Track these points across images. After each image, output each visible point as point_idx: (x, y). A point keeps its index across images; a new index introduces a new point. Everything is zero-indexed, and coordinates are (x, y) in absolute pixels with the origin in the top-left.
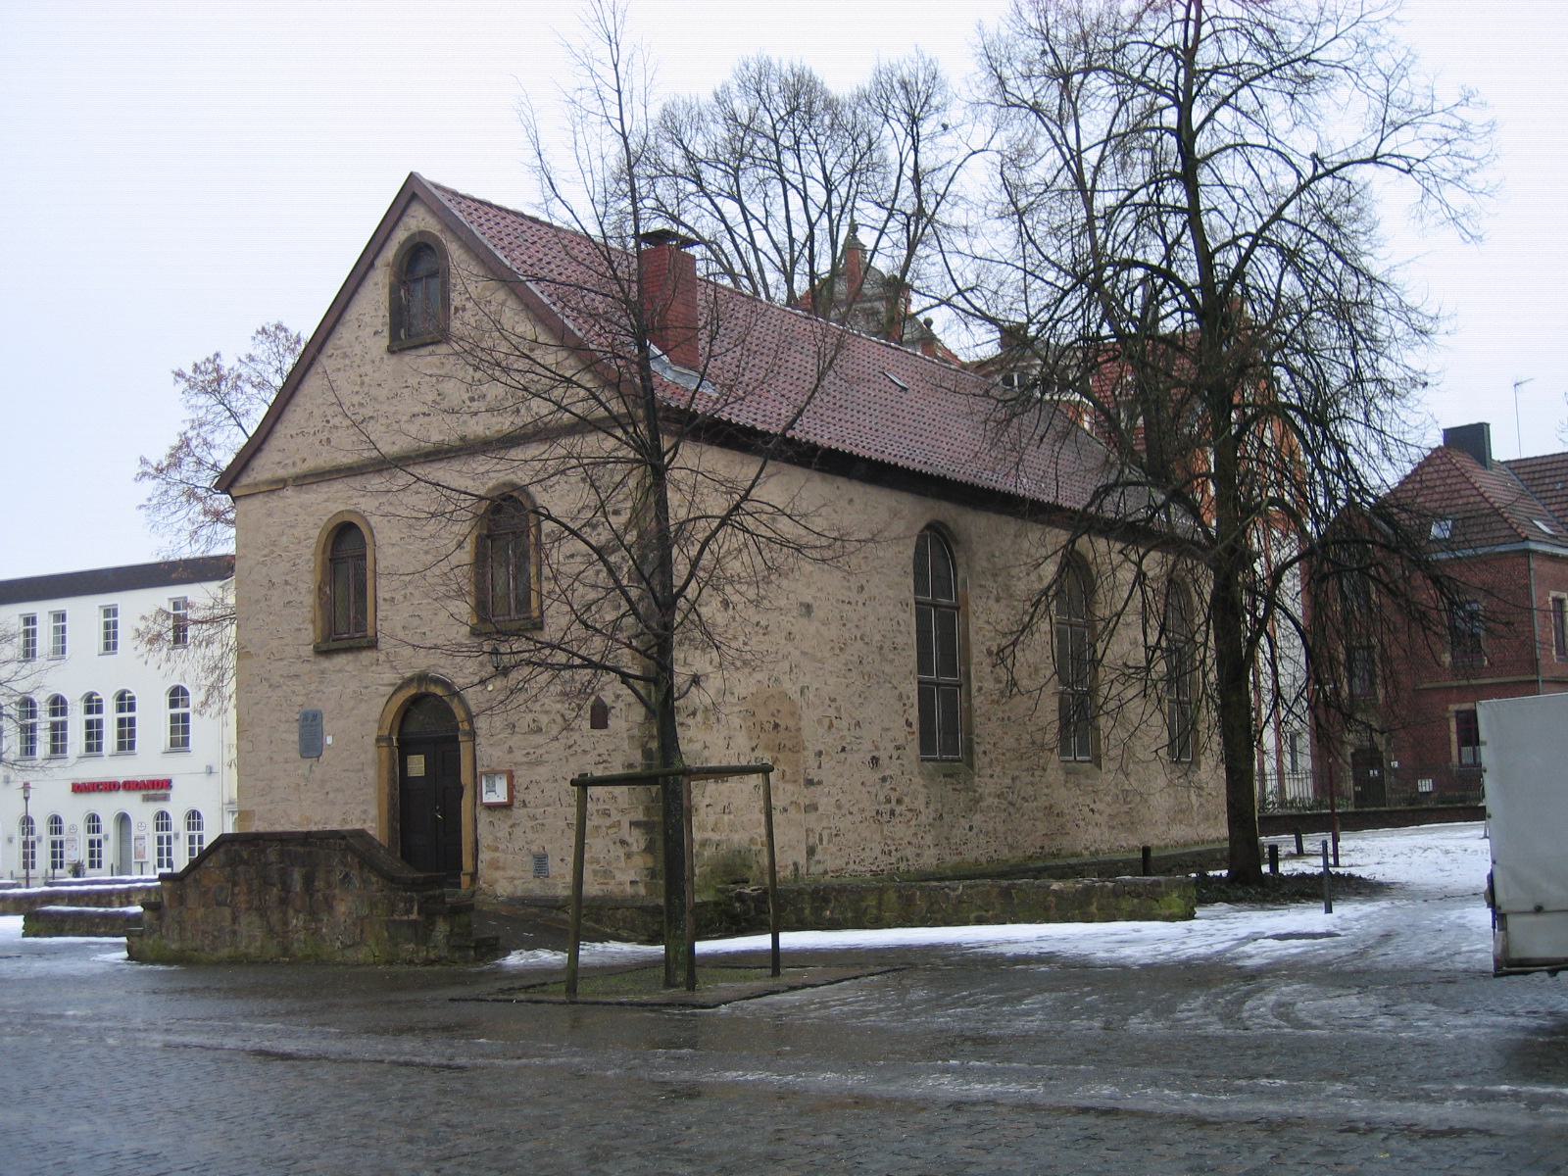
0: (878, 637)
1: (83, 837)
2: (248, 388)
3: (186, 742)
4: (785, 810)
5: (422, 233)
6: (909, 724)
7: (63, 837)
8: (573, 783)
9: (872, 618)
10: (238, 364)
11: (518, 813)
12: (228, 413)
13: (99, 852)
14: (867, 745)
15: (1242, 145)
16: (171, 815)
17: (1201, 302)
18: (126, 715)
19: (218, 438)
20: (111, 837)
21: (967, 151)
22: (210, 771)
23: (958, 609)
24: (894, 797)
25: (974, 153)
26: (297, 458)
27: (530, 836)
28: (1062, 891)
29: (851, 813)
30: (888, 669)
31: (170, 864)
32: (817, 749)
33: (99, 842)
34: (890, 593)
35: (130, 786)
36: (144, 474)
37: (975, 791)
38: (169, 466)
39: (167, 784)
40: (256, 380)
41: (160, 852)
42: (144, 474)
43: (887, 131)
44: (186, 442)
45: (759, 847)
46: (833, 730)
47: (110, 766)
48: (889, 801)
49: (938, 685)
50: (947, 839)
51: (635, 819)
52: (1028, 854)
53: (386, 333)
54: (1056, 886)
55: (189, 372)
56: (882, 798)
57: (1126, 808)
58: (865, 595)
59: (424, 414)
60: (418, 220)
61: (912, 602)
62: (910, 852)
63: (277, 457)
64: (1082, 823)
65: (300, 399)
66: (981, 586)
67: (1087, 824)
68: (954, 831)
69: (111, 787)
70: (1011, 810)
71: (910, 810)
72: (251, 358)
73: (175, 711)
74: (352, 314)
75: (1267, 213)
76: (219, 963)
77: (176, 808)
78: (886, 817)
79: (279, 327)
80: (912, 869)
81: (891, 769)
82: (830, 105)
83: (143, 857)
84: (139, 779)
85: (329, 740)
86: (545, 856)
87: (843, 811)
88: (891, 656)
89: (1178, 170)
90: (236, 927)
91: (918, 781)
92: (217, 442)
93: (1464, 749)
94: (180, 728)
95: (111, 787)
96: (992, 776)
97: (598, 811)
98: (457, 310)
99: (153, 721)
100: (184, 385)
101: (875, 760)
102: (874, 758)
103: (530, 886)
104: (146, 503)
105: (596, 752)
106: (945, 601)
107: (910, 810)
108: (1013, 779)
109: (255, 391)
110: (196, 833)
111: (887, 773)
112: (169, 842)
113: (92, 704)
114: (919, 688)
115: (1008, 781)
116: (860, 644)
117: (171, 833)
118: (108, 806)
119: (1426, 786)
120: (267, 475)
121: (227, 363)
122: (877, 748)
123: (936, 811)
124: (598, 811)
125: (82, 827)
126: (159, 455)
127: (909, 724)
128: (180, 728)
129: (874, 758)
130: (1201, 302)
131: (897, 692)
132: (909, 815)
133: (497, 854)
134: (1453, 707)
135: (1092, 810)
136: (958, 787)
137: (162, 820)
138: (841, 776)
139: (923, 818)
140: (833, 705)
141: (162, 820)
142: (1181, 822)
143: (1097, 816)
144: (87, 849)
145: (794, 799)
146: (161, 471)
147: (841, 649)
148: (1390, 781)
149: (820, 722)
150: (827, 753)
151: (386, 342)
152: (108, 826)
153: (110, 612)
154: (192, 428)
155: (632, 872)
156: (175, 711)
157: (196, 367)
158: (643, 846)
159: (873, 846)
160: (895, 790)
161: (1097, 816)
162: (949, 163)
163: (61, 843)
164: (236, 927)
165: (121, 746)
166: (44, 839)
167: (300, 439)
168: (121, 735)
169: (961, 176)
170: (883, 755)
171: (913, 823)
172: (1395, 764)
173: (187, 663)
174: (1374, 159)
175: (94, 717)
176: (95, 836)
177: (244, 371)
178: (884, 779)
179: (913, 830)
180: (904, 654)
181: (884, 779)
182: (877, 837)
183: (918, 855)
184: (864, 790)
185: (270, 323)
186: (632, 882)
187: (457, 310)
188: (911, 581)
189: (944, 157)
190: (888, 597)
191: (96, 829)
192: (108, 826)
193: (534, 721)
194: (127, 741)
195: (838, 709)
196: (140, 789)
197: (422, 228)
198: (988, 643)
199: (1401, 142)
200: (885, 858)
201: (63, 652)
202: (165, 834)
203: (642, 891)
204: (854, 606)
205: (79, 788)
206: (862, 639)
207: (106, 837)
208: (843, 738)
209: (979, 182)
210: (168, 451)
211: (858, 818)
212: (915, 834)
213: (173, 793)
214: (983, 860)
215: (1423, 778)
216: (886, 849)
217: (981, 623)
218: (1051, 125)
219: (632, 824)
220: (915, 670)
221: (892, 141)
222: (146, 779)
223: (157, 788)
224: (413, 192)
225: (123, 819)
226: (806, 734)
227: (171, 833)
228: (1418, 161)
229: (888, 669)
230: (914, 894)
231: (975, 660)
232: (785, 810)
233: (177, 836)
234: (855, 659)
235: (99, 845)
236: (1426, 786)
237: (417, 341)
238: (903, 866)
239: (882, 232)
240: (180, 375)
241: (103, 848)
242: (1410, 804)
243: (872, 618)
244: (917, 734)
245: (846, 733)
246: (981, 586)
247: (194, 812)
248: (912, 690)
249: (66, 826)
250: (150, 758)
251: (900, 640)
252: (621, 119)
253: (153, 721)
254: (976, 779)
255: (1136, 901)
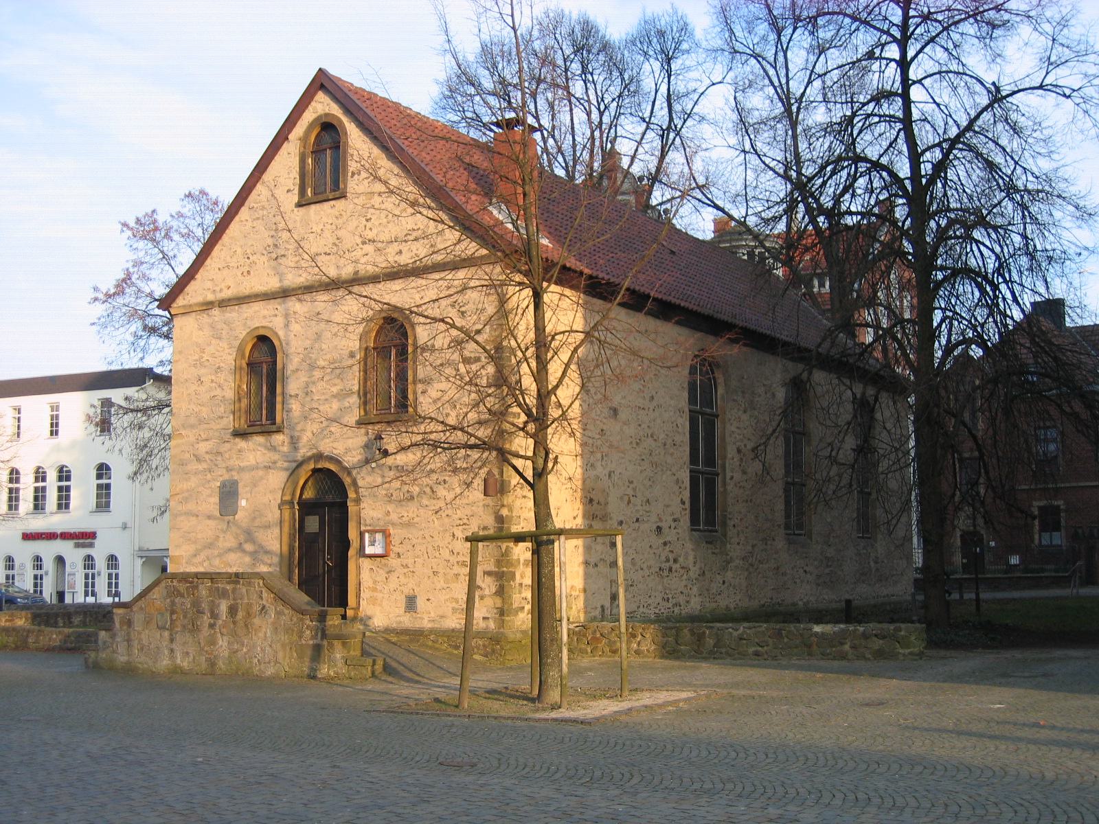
0: (662, 436)
1: (30, 573)
2: (176, 237)
3: (108, 505)
4: (596, 565)
5: (327, 115)
6: (683, 503)
7: (15, 572)
8: (467, 539)
9: (659, 421)
10: (169, 219)
11: (392, 561)
12: (161, 256)
13: (41, 584)
14: (654, 518)
15: (947, 72)
16: (95, 556)
17: (910, 189)
18: (64, 483)
19: (153, 273)
20: (51, 572)
21: (708, 82)
22: (125, 527)
23: (717, 416)
24: (671, 557)
25: (713, 84)
26: (223, 286)
27: (403, 579)
28: (823, 633)
29: (642, 569)
30: (669, 460)
31: (117, 594)
32: (620, 519)
33: (41, 576)
34: (672, 402)
35: (65, 536)
36: (96, 299)
37: (727, 555)
38: (114, 294)
39: (92, 535)
40: (185, 231)
41: (86, 585)
42: (96, 299)
43: (646, 66)
44: (128, 276)
45: (577, 593)
46: (631, 505)
47: (53, 521)
48: (668, 560)
49: (703, 473)
50: (708, 590)
51: (488, 569)
52: (762, 602)
53: (296, 191)
54: (817, 629)
55: (132, 224)
56: (663, 558)
57: (827, 571)
58: (655, 403)
59: (325, 254)
60: (323, 105)
61: (687, 410)
62: (682, 599)
63: (209, 284)
64: (798, 581)
65: (226, 238)
66: (734, 400)
67: (802, 582)
68: (712, 585)
69: (51, 536)
70: (751, 569)
71: (683, 568)
72: (180, 215)
73: (100, 482)
74: (268, 176)
75: (964, 124)
76: (50, 650)
77: (99, 553)
78: (666, 573)
79: (203, 193)
80: (683, 612)
81: (670, 535)
82: (605, 47)
83: (74, 588)
84: (72, 531)
85: (243, 503)
86: (415, 597)
87: (637, 567)
88: (672, 450)
89: (900, 91)
90: (174, 646)
91: (689, 546)
92: (152, 276)
93: (1043, 534)
94: (104, 492)
95: (51, 536)
96: (738, 544)
97: (458, 562)
98: (353, 174)
99: (83, 492)
100: (129, 233)
101: (659, 529)
102: (658, 527)
103: (402, 619)
104: (96, 321)
105: (457, 516)
106: (708, 410)
107: (683, 568)
108: (753, 546)
109: (182, 239)
110: (114, 572)
111: (668, 539)
112: (93, 578)
113: (40, 475)
114: (691, 476)
115: (749, 548)
116: (650, 440)
117: (96, 571)
118: (49, 551)
119: (1015, 560)
120: (200, 299)
121: (161, 218)
122: (661, 520)
123: (701, 568)
124: (458, 562)
125: (29, 565)
126: (109, 285)
127: (683, 503)
128: (104, 492)
129: (658, 527)
130: (910, 189)
131: (675, 478)
132: (682, 571)
133: (375, 594)
134: (1036, 504)
135: (805, 571)
136: (716, 551)
137: (89, 562)
138: (635, 540)
139: (691, 573)
140: (631, 486)
141: (89, 562)
142: (863, 582)
143: (808, 576)
144: (32, 581)
145: (603, 557)
146: (110, 296)
147: (637, 444)
148: (988, 557)
149: (621, 498)
150: (626, 523)
151: (296, 199)
152: (49, 565)
153: (55, 408)
154: (134, 266)
155: (485, 610)
156: (100, 482)
157: (138, 221)
158: (494, 590)
159: (657, 594)
160: (672, 552)
161: (808, 576)
162: (695, 90)
163: (13, 576)
164: (174, 646)
165: (60, 506)
166: (102, 574)
167: (226, 272)
168: (60, 498)
169: (703, 101)
170: (664, 525)
171: (685, 577)
172: (993, 544)
173: (124, 441)
174: (1041, 87)
175: (14, 486)
176: (39, 572)
177: (175, 224)
178: (665, 544)
179: (684, 583)
180: (681, 449)
181: (665, 544)
182: (660, 588)
183: (688, 602)
184: (651, 552)
185: (195, 188)
186: (484, 618)
187: (353, 174)
188: (686, 395)
189: (692, 86)
190: (670, 405)
191: (40, 567)
192: (49, 565)
193: (408, 491)
194: (64, 503)
195: (634, 489)
196: (73, 539)
197: (327, 111)
198: (738, 444)
199: (1066, 77)
200: (665, 603)
201: (18, 436)
202: (90, 572)
203: (492, 625)
204: (646, 411)
205: (27, 537)
206: (652, 436)
207: (47, 574)
208: (637, 511)
209: (717, 103)
210: (114, 283)
211: (647, 572)
212: (686, 586)
213: (96, 542)
214: (732, 606)
215: (1012, 554)
216: (666, 597)
217: (733, 429)
218: (768, 67)
219: (485, 573)
220: (688, 462)
221: (650, 73)
222: (77, 531)
223: (85, 538)
224: (322, 83)
225: (60, 561)
226: (610, 508)
227: (96, 571)
228: (1074, 90)
229: (669, 460)
230: (704, 633)
231: (729, 456)
232: (596, 565)
233: (99, 574)
234: (646, 451)
235: (41, 579)
236: (1015, 560)
237: (321, 197)
238: (677, 610)
239: (640, 143)
240: (125, 225)
241: (44, 581)
242: (1006, 573)
243: (659, 421)
244: (688, 511)
245: (639, 507)
246: (734, 400)
247: (112, 556)
248: (685, 476)
249: (17, 564)
250: (80, 515)
251: (678, 439)
252: (512, 16)
253: (83, 492)
254: (728, 546)
255: (881, 642)
